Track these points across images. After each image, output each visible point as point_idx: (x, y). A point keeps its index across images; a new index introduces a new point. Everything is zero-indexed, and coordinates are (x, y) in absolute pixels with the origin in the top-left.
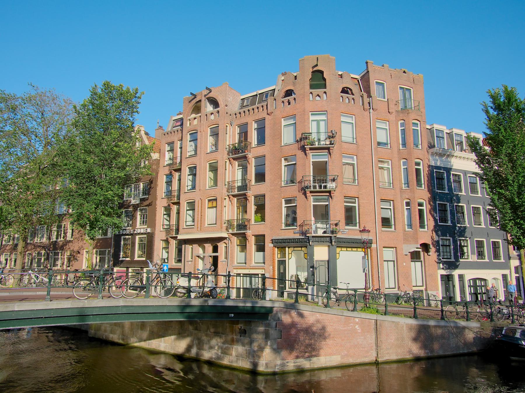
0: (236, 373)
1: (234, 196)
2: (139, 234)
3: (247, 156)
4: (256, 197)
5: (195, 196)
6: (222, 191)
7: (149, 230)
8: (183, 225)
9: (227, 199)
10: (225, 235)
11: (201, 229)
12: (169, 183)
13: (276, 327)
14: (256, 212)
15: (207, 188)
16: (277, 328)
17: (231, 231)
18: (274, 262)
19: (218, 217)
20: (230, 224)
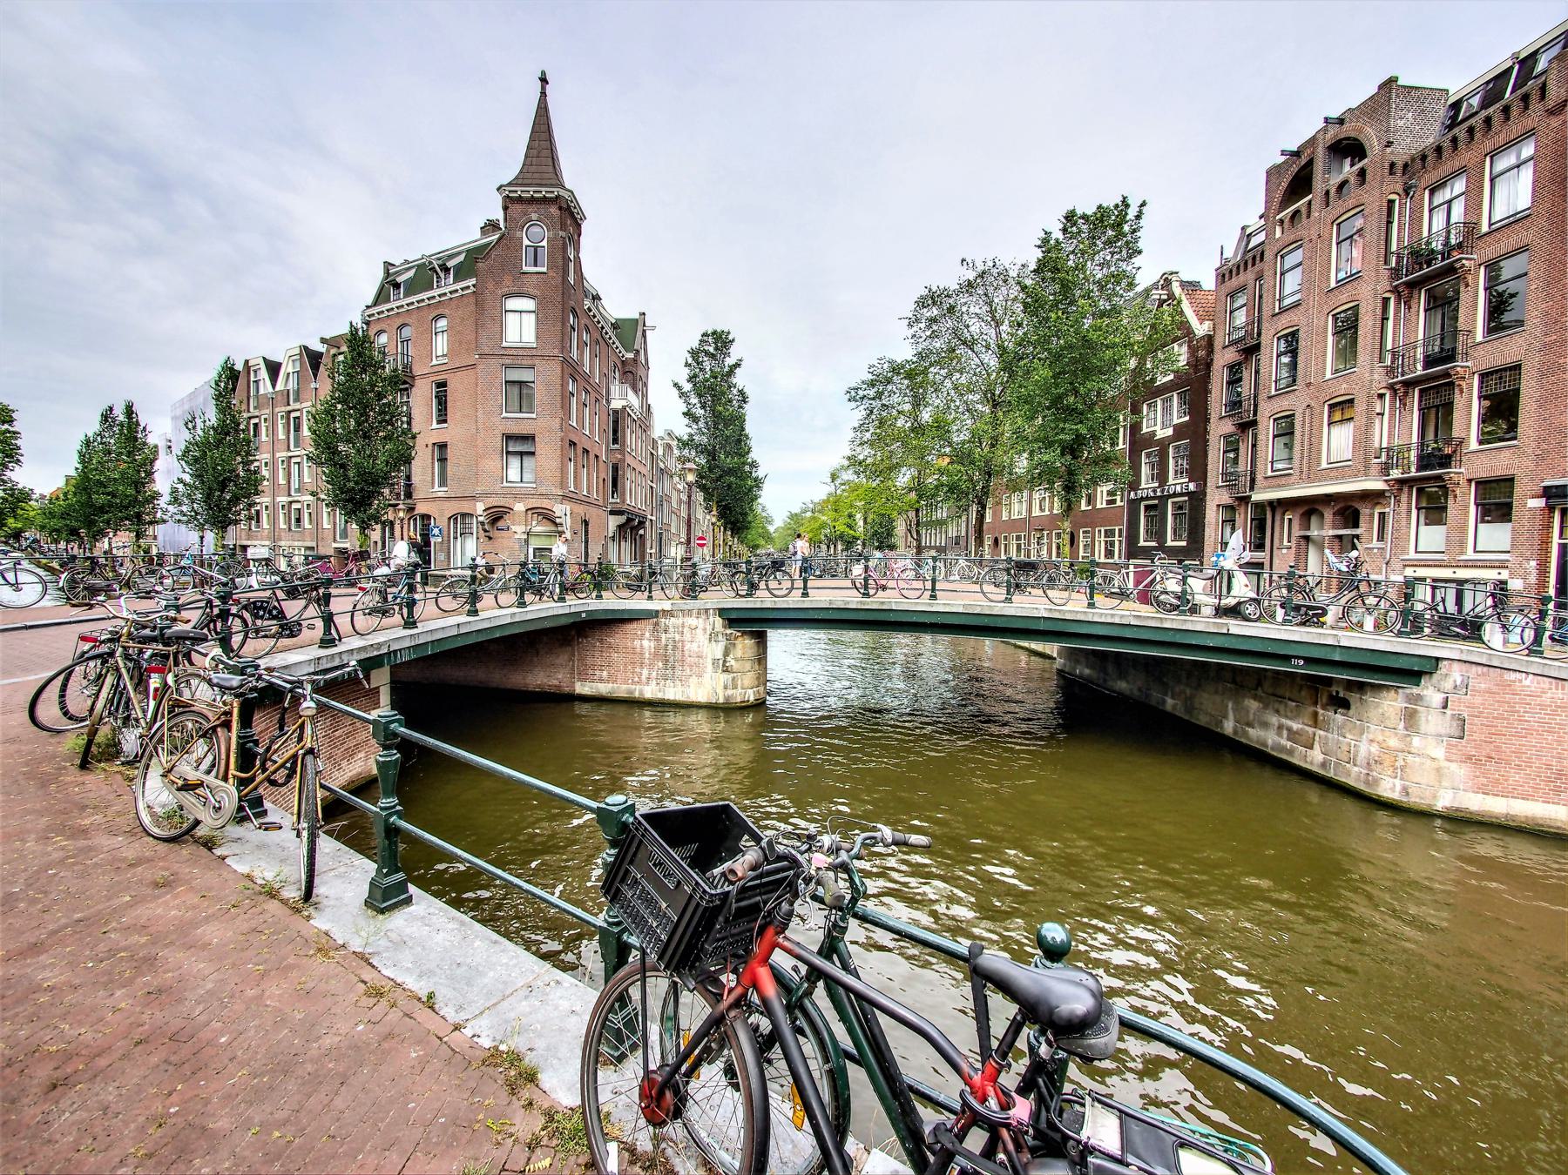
0: (674, 719)
1: (1408, 384)
2: (1175, 495)
3: (1458, 265)
4: (1484, 376)
5: (1295, 403)
6: (1369, 374)
7: (1192, 487)
8: (1264, 470)
9: (1388, 397)
10: (1378, 485)
11: (1311, 476)
12: (1234, 381)
13: (1445, 707)
14: (1485, 419)
15: (1328, 375)
16: (1448, 712)
17: (1396, 474)
18: (1547, 552)
19: (1362, 441)
20: (1392, 458)
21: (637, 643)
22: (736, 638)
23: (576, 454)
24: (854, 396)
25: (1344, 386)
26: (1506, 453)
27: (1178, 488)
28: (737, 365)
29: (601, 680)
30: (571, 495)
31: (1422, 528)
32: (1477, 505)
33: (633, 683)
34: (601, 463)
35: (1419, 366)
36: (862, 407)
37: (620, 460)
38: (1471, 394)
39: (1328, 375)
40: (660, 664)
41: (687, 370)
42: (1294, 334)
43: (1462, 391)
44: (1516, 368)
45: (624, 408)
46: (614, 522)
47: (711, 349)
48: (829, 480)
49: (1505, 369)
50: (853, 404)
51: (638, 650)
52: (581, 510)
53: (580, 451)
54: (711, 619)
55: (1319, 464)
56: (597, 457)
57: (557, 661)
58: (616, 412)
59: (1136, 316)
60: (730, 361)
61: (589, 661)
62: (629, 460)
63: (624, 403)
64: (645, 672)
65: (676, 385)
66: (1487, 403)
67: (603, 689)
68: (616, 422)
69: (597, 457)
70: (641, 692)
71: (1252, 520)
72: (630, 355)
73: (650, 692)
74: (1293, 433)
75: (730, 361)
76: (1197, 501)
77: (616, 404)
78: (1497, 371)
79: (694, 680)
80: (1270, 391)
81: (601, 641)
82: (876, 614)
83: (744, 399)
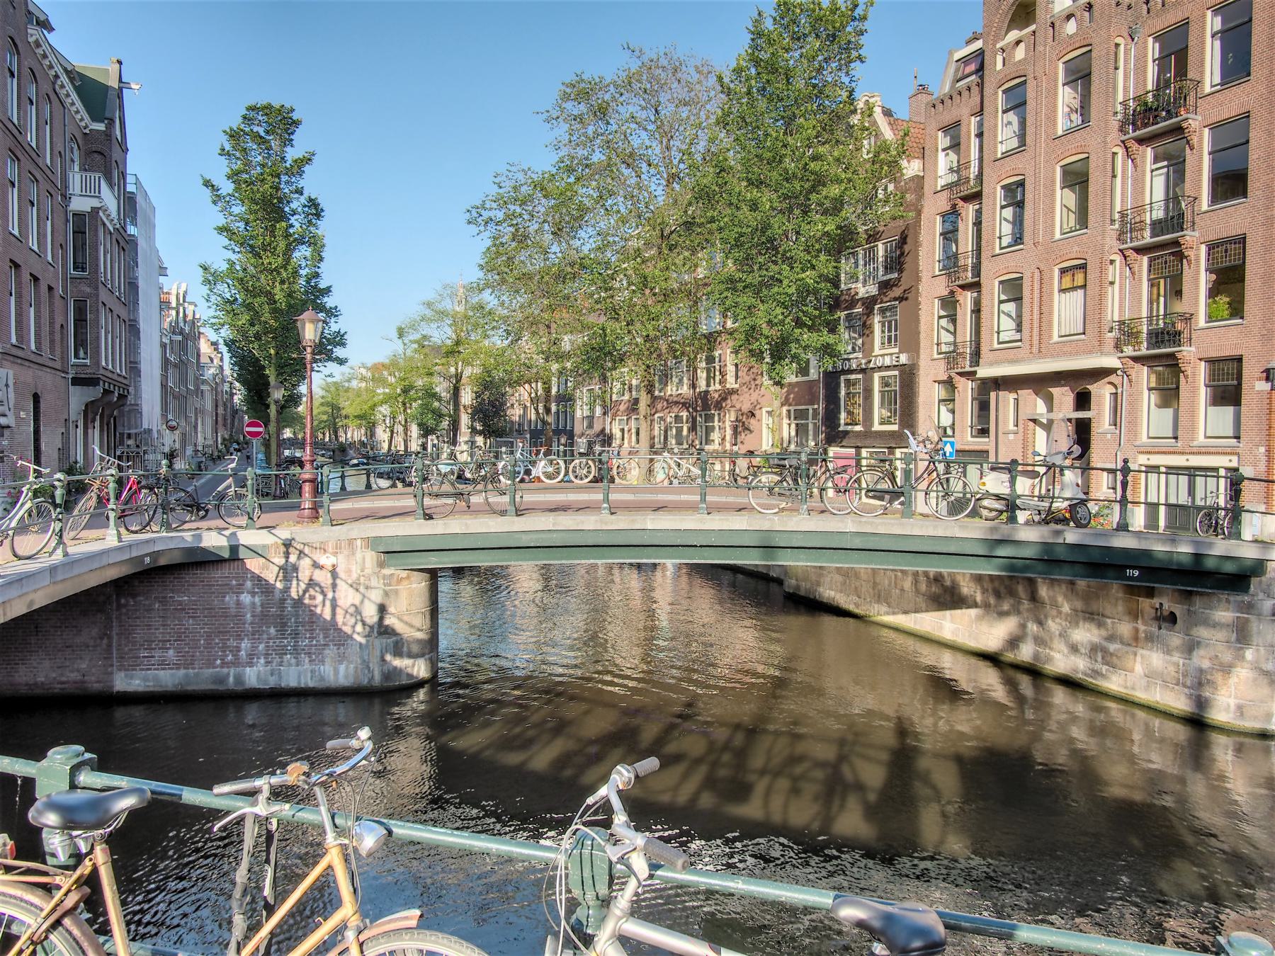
1: (1140, 250)
3: (1185, 125)
4: (1212, 247)
7: (904, 359)
8: (989, 342)
14: (1213, 293)
15: (1058, 236)
17: (1129, 351)
19: (1092, 314)
20: (1127, 332)
21: (230, 599)
22: (400, 580)
23: (19, 284)
24: (476, 217)
25: (1076, 248)
26: (1234, 331)
27: (887, 361)
28: (307, 160)
29: (163, 664)
30: (32, 357)
31: (1211, 409)
32: (1206, 386)
33: (224, 664)
34: (57, 298)
35: (1147, 233)
36: (488, 234)
37: (89, 296)
38: (1198, 266)
39: (1058, 236)
40: (272, 630)
41: (223, 161)
42: (1021, 184)
43: (1189, 263)
44: (1242, 240)
45: (95, 210)
46: (78, 398)
47: (261, 131)
48: (396, 335)
49: (1230, 242)
50: (473, 229)
51: (233, 611)
52: (29, 375)
53: (26, 277)
54: (359, 555)
55: (1050, 337)
56: (50, 288)
57: (78, 640)
58: (78, 216)
59: (857, 150)
60: (292, 154)
61: (139, 634)
62: (103, 295)
63: (95, 203)
64: (245, 644)
65: (207, 184)
66: (1214, 277)
67: (167, 679)
68: (79, 232)
69: (50, 288)
70: (239, 679)
71: (973, 399)
72: (101, 127)
73: (254, 676)
74: (1021, 299)
75: (292, 154)
76: (908, 376)
77: (80, 204)
78: (1222, 244)
79: (330, 652)
80: (993, 249)
81: (163, 601)
82: (534, 536)
83: (315, 210)
